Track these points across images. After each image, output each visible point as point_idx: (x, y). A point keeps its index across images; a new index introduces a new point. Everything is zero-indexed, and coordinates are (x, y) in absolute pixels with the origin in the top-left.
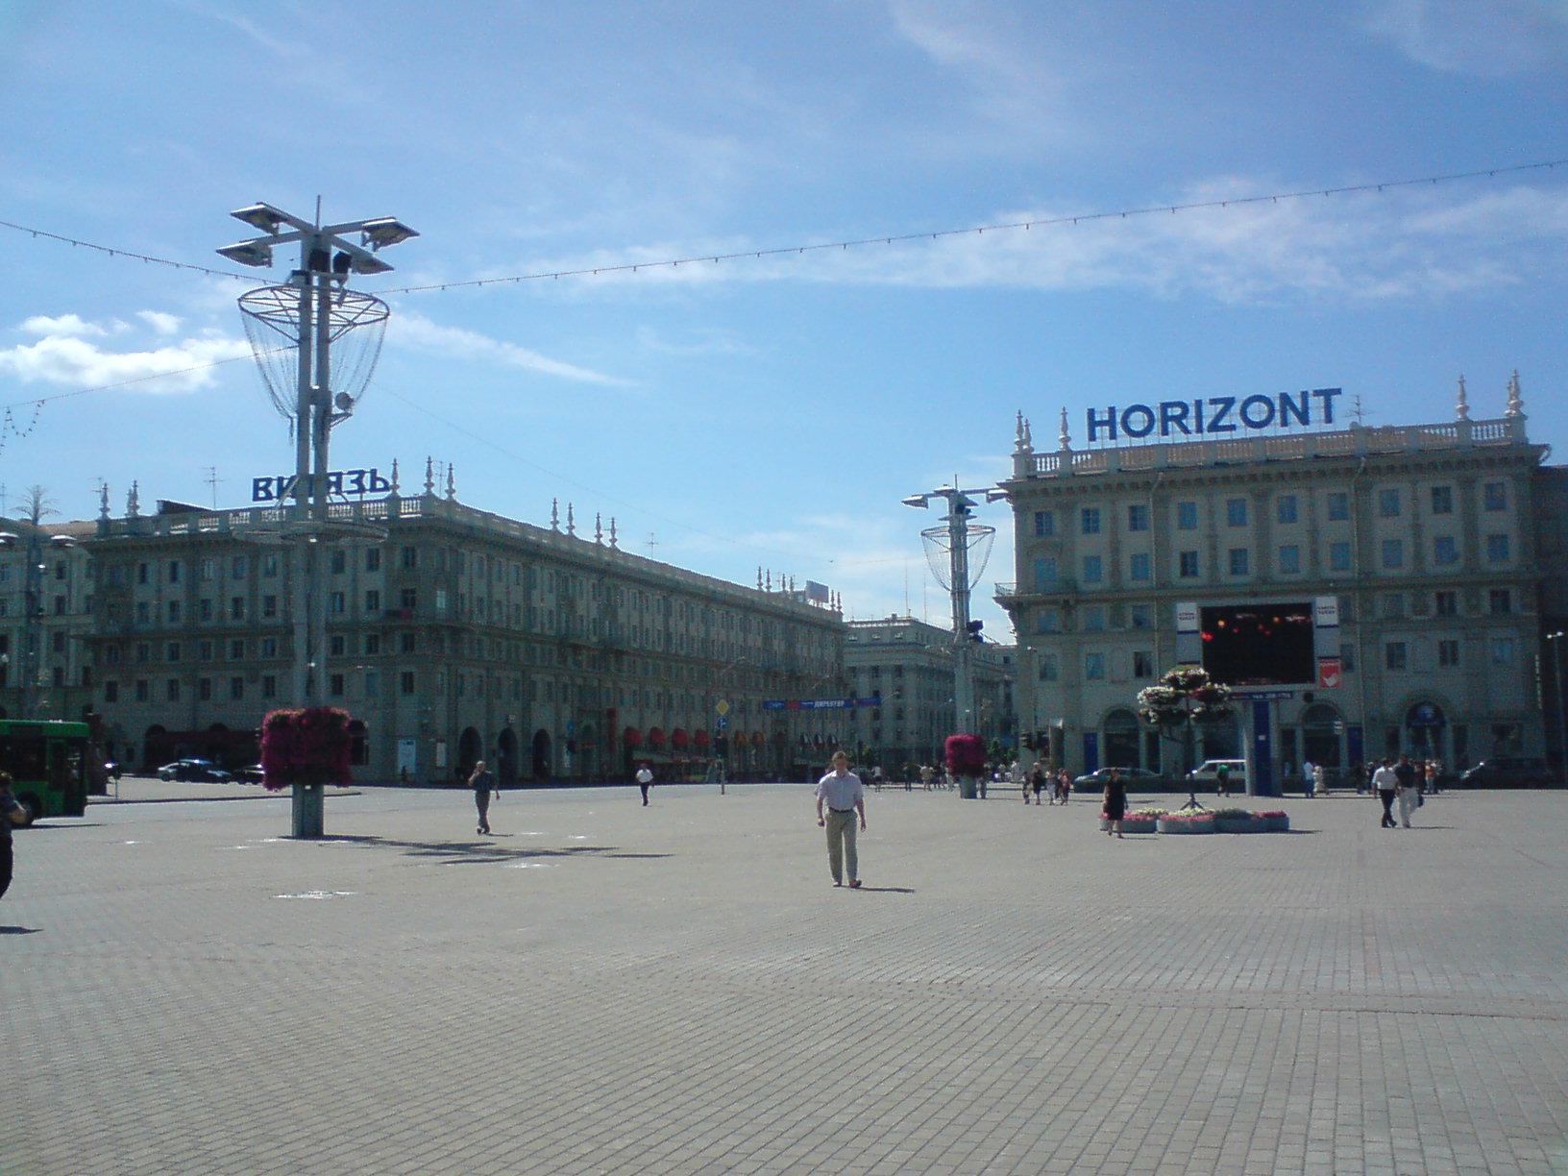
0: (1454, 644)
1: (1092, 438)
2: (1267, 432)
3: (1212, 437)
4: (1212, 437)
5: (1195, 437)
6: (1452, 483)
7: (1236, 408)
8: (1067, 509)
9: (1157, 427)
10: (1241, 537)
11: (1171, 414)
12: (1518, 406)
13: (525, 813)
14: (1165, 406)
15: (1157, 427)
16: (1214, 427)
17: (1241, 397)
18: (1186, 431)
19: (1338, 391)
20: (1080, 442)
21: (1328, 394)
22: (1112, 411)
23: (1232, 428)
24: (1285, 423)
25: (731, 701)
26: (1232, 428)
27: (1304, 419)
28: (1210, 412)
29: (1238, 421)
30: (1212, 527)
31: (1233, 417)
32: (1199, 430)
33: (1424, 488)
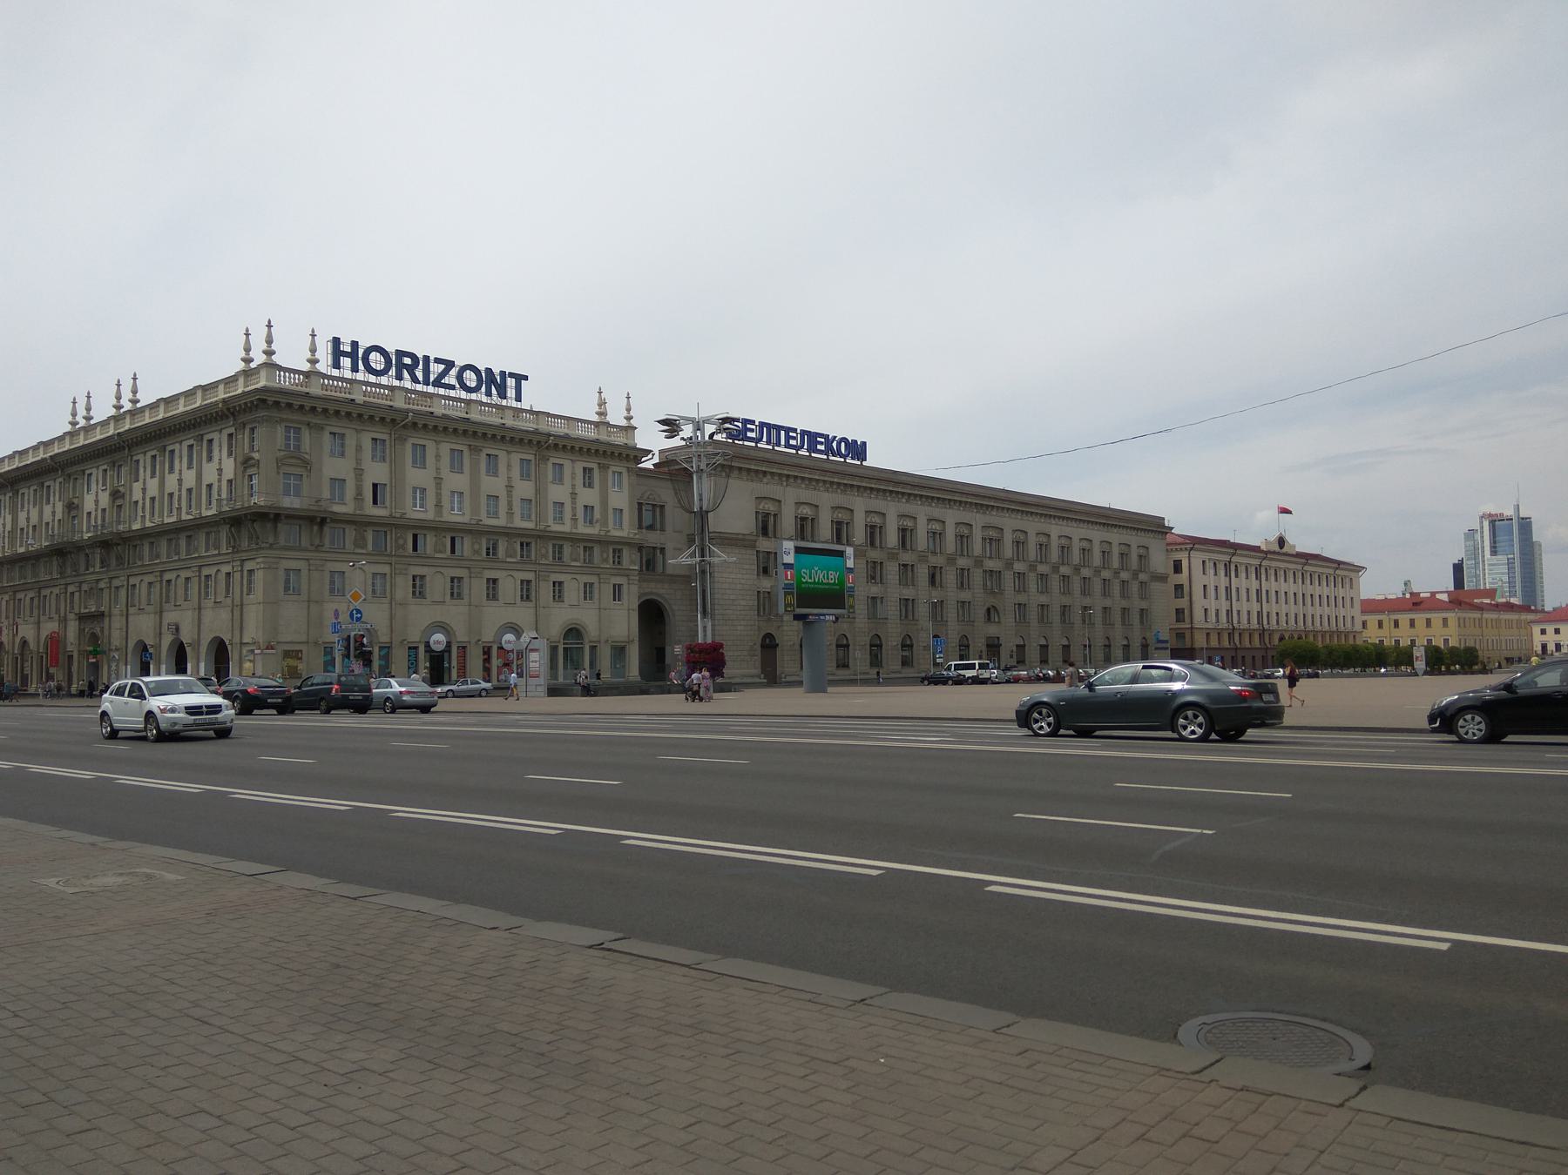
0: (592, 584)
1: (336, 365)
2: (384, 380)
3: (431, 389)
4: (431, 389)
5: (419, 387)
6: (595, 466)
7: (453, 372)
8: (474, 450)
9: (393, 372)
10: (589, 496)
11: (404, 362)
12: (629, 418)
13: (1256, 530)
14: (401, 354)
15: (393, 372)
16: (438, 383)
17: (460, 363)
18: (415, 380)
19: (526, 378)
20: (324, 366)
21: (520, 378)
22: (355, 344)
23: (453, 387)
24: (489, 394)
25: (788, 566)
26: (453, 387)
27: (503, 395)
28: (436, 369)
29: (453, 381)
30: (509, 478)
31: (451, 379)
32: (426, 382)
33: (579, 467)
